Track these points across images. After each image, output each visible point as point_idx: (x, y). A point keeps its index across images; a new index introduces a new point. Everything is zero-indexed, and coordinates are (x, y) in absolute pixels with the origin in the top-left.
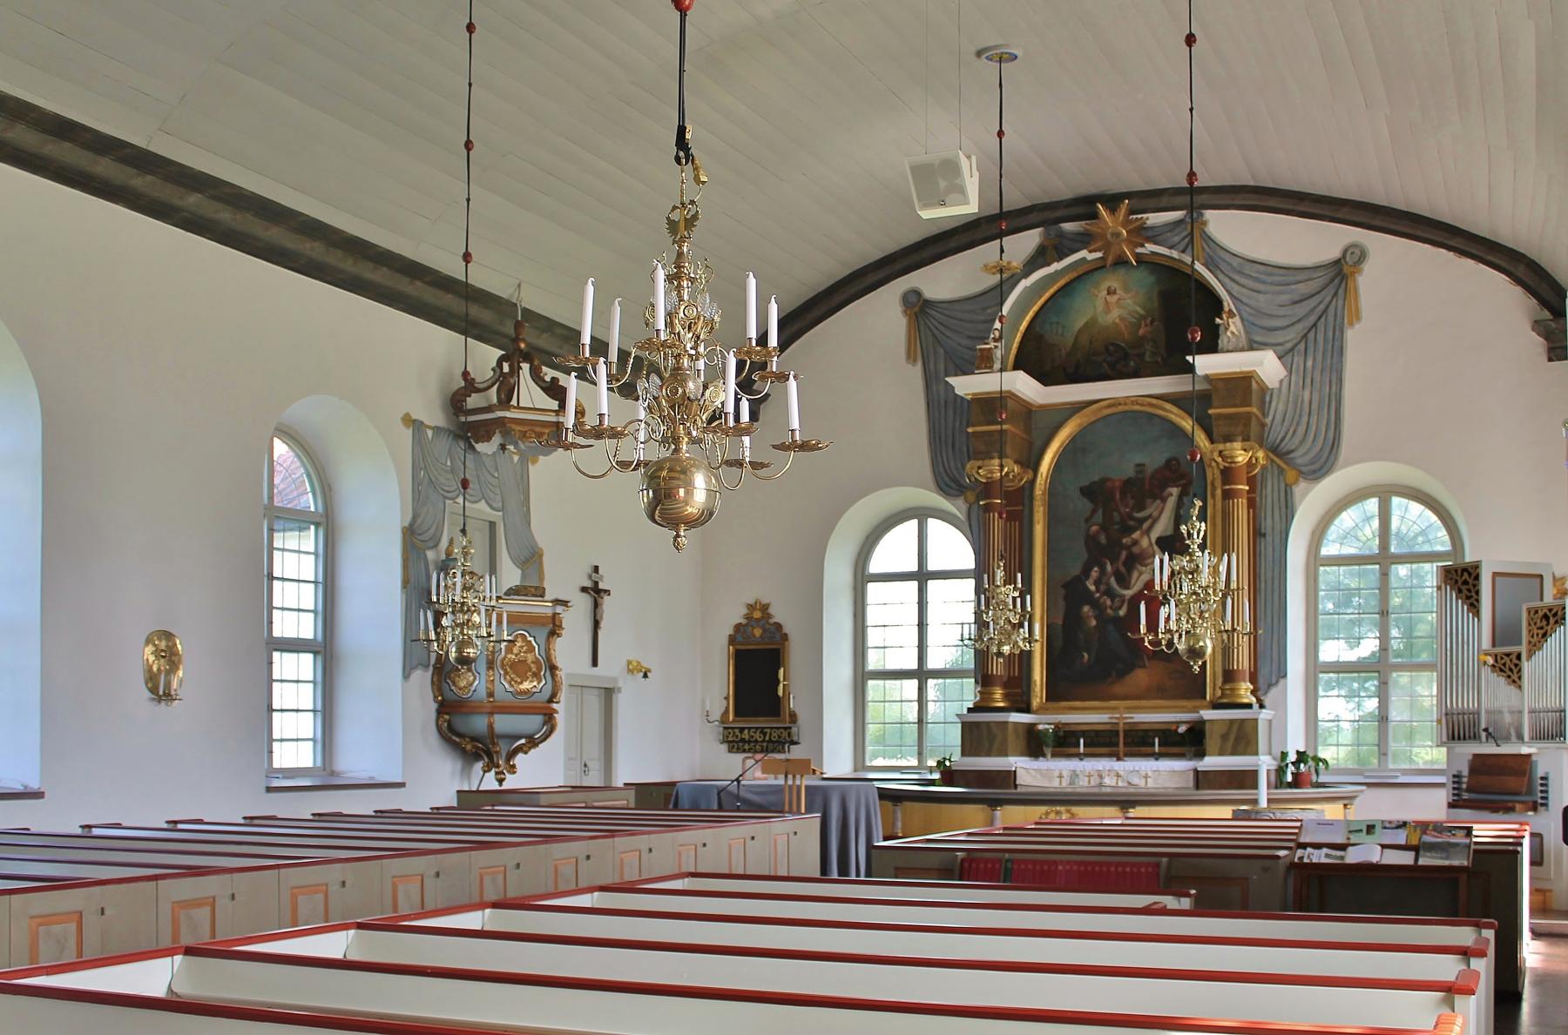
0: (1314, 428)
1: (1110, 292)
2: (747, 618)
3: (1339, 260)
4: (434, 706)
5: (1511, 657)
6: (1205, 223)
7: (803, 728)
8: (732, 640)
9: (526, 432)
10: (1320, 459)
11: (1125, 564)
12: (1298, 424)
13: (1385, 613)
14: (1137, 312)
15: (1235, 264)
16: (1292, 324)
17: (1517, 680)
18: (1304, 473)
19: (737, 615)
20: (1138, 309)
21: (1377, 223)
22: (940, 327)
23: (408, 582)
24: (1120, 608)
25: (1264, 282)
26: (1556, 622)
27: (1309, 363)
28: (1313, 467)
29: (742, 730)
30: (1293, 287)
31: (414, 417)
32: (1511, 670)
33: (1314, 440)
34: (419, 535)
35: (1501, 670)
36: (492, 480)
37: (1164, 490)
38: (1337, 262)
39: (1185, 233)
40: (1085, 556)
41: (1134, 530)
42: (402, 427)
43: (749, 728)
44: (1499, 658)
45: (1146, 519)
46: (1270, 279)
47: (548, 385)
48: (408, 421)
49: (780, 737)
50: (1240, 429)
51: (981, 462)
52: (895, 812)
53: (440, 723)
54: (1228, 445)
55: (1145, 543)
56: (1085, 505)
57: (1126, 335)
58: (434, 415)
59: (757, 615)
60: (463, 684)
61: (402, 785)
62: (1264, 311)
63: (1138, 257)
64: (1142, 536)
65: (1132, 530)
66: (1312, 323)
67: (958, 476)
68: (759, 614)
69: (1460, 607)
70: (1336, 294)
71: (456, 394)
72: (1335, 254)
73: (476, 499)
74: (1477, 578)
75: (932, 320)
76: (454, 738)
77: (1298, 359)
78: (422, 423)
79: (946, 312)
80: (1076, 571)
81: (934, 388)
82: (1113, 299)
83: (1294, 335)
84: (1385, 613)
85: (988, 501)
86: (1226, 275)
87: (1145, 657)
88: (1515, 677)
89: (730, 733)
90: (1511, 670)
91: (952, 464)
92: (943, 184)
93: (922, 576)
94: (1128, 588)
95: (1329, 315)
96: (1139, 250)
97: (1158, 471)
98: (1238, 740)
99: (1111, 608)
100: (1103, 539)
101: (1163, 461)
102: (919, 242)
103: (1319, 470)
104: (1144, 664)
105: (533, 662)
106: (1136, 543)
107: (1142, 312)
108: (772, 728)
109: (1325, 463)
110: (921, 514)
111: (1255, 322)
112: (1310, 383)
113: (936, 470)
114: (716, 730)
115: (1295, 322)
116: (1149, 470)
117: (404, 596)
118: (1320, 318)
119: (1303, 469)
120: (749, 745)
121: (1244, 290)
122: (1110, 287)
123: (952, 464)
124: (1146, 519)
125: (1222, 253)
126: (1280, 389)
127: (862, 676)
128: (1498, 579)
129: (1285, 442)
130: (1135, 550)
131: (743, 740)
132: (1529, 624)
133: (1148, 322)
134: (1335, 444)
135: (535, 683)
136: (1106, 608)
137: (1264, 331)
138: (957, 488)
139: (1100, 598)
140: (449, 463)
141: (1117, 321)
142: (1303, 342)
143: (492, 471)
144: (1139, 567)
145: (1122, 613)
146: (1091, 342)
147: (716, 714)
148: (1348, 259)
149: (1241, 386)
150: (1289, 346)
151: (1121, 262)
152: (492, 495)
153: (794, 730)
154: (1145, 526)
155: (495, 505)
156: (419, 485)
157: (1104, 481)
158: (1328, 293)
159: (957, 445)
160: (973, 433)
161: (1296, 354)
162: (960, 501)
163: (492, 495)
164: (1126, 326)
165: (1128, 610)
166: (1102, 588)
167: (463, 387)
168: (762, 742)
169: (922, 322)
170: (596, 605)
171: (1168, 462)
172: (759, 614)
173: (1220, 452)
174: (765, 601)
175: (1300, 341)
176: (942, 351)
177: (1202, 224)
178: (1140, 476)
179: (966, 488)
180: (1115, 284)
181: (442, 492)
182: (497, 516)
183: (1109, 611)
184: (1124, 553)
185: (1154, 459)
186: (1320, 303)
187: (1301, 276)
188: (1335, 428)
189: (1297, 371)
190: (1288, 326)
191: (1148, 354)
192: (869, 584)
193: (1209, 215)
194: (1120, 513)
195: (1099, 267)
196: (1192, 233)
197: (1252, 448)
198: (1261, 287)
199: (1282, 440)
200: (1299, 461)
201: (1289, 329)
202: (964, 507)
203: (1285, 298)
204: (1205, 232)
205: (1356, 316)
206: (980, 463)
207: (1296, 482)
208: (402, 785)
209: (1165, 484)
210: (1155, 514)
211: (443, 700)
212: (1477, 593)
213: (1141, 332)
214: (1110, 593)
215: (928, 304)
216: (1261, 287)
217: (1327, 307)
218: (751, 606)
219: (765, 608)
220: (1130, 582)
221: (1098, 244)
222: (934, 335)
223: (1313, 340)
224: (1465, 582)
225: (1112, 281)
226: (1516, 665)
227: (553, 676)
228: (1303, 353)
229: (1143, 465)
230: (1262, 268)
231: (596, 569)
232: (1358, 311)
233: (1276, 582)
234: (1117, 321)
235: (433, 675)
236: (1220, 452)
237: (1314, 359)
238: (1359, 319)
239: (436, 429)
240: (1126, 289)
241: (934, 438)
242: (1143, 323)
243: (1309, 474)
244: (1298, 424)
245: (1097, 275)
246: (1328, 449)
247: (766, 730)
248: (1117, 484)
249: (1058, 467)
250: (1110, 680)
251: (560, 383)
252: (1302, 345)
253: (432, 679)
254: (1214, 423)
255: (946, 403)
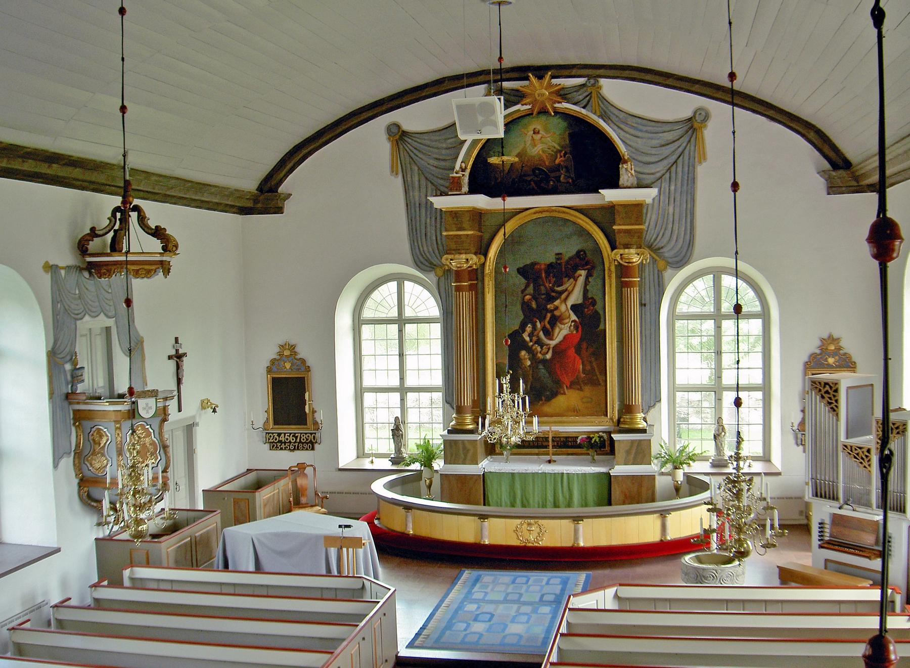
0: (676, 232)
1: (536, 132)
2: (280, 355)
3: (691, 118)
4: (76, 481)
5: (863, 450)
6: (600, 88)
7: (324, 434)
8: (269, 370)
9: (138, 270)
10: (681, 253)
11: (549, 323)
12: (665, 229)
13: (719, 353)
14: (555, 148)
15: (621, 117)
16: (661, 160)
17: (866, 464)
18: (669, 263)
19: (271, 353)
20: (556, 146)
21: (718, 96)
22: (415, 151)
23: (53, 394)
24: (547, 353)
25: (641, 131)
26: (898, 433)
27: (673, 188)
28: (674, 259)
29: (279, 435)
30: (661, 135)
31: (51, 263)
32: (862, 458)
33: (676, 241)
34: (60, 354)
35: (855, 457)
36: (109, 296)
37: (575, 273)
38: (690, 119)
39: (587, 94)
40: (522, 317)
41: (555, 299)
42: (44, 273)
43: (285, 434)
44: (853, 449)
45: (563, 292)
46: (644, 129)
47: (153, 231)
48: (51, 268)
49: (307, 440)
50: (635, 240)
51: (453, 256)
52: (407, 516)
53: (81, 494)
54: (626, 250)
55: (563, 308)
56: (521, 281)
57: (547, 163)
58: (66, 257)
59: (287, 353)
60: (98, 465)
61: (58, 550)
62: (642, 150)
63: (554, 109)
64: (561, 303)
65: (552, 300)
66: (674, 160)
67: (430, 258)
68: (288, 351)
69: (822, 408)
70: (689, 141)
71: (80, 241)
72: (688, 114)
73: (97, 314)
74: (836, 391)
75: (409, 145)
76: (92, 503)
77: (665, 185)
78: (57, 266)
79: (418, 140)
80: (517, 327)
81: (411, 195)
82: (537, 137)
83: (661, 168)
84: (719, 353)
85: (458, 284)
86: (615, 124)
87: (565, 388)
88: (866, 464)
89: (270, 436)
90: (862, 458)
91: (425, 248)
92: (480, 119)
93: (401, 321)
94: (551, 339)
95: (685, 157)
96: (557, 105)
97: (570, 258)
98: (637, 454)
99: (540, 352)
100: (534, 305)
101: (574, 252)
102: (401, 92)
103: (681, 262)
104: (564, 392)
105: (150, 444)
106: (557, 308)
107: (559, 148)
108: (301, 433)
109: (684, 256)
110: (400, 279)
111: (635, 158)
112: (673, 201)
113: (414, 253)
114: (258, 438)
115: (663, 159)
116: (566, 258)
117: (51, 405)
118: (679, 157)
119: (670, 260)
120: (285, 445)
121: (628, 136)
122: (535, 129)
123: (425, 248)
124: (563, 292)
125: (612, 109)
126: (653, 204)
127: (360, 392)
128: (849, 391)
129: (657, 242)
130: (557, 313)
131: (280, 442)
132: (878, 431)
133: (562, 154)
134: (691, 244)
135: (153, 461)
136: (537, 353)
137: (642, 164)
138: (429, 265)
139: (533, 345)
140: (77, 292)
141: (541, 152)
142: (668, 173)
143: (106, 288)
144: (559, 324)
145: (548, 356)
146: (522, 167)
147: (260, 423)
148: (697, 119)
149: (636, 210)
150: (658, 175)
151: (543, 112)
152: (108, 308)
153: (317, 435)
154: (563, 296)
155: (110, 314)
156: (57, 315)
157: (533, 264)
158: (685, 139)
159: (429, 234)
160: (446, 236)
161: (663, 180)
162: (432, 275)
163: (108, 308)
164: (547, 156)
165: (553, 355)
166: (535, 339)
167: (88, 234)
168: (294, 443)
169: (401, 147)
170: (178, 367)
171: (578, 252)
172: (288, 351)
173: (621, 255)
174: (292, 342)
175: (666, 172)
176: (416, 168)
177: (598, 88)
178: (559, 262)
179: (435, 265)
180: (539, 127)
181: (73, 315)
182: (110, 322)
183: (539, 355)
184: (549, 315)
185: (569, 249)
186: (679, 147)
187: (667, 128)
188: (691, 233)
189: (664, 193)
190: (659, 161)
191: (563, 176)
192: (363, 326)
193: (602, 81)
194: (545, 287)
195: (529, 114)
196: (591, 96)
197: (643, 254)
198: (639, 134)
199: (655, 240)
200: (666, 255)
201: (659, 163)
202: (435, 279)
203: (655, 142)
204: (599, 93)
205: (703, 157)
206: (450, 257)
207: (665, 269)
208: (58, 550)
209: (576, 268)
210: (570, 288)
211: (83, 476)
212: (836, 401)
213: (557, 161)
214: (539, 342)
215: (404, 134)
216: (639, 134)
217: (685, 148)
218: (282, 346)
219: (292, 348)
220: (553, 335)
221: (528, 100)
222: (410, 156)
223: (675, 172)
224: (827, 392)
225: (537, 124)
226: (867, 456)
227: (166, 453)
228: (668, 180)
229: (561, 254)
230: (640, 121)
231: (177, 339)
232: (704, 154)
233: (653, 336)
234: (541, 152)
235: (74, 458)
236: (621, 255)
237: (676, 185)
238: (705, 159)
239: (68, 268)
240: (546, 130)
241: (412, 229)
242: (559, 156)
243: (673, 264)
244: (665, 229)
245: (526, 120)
246: (686, 248)
247: (296, 435)
248: (543, 267)
249: (501, 253)
250: (541, 402)
251: (167, 233)
252: (667, 175)
253: (74, 461)
254: (617, 236)
255: (420, 204)
